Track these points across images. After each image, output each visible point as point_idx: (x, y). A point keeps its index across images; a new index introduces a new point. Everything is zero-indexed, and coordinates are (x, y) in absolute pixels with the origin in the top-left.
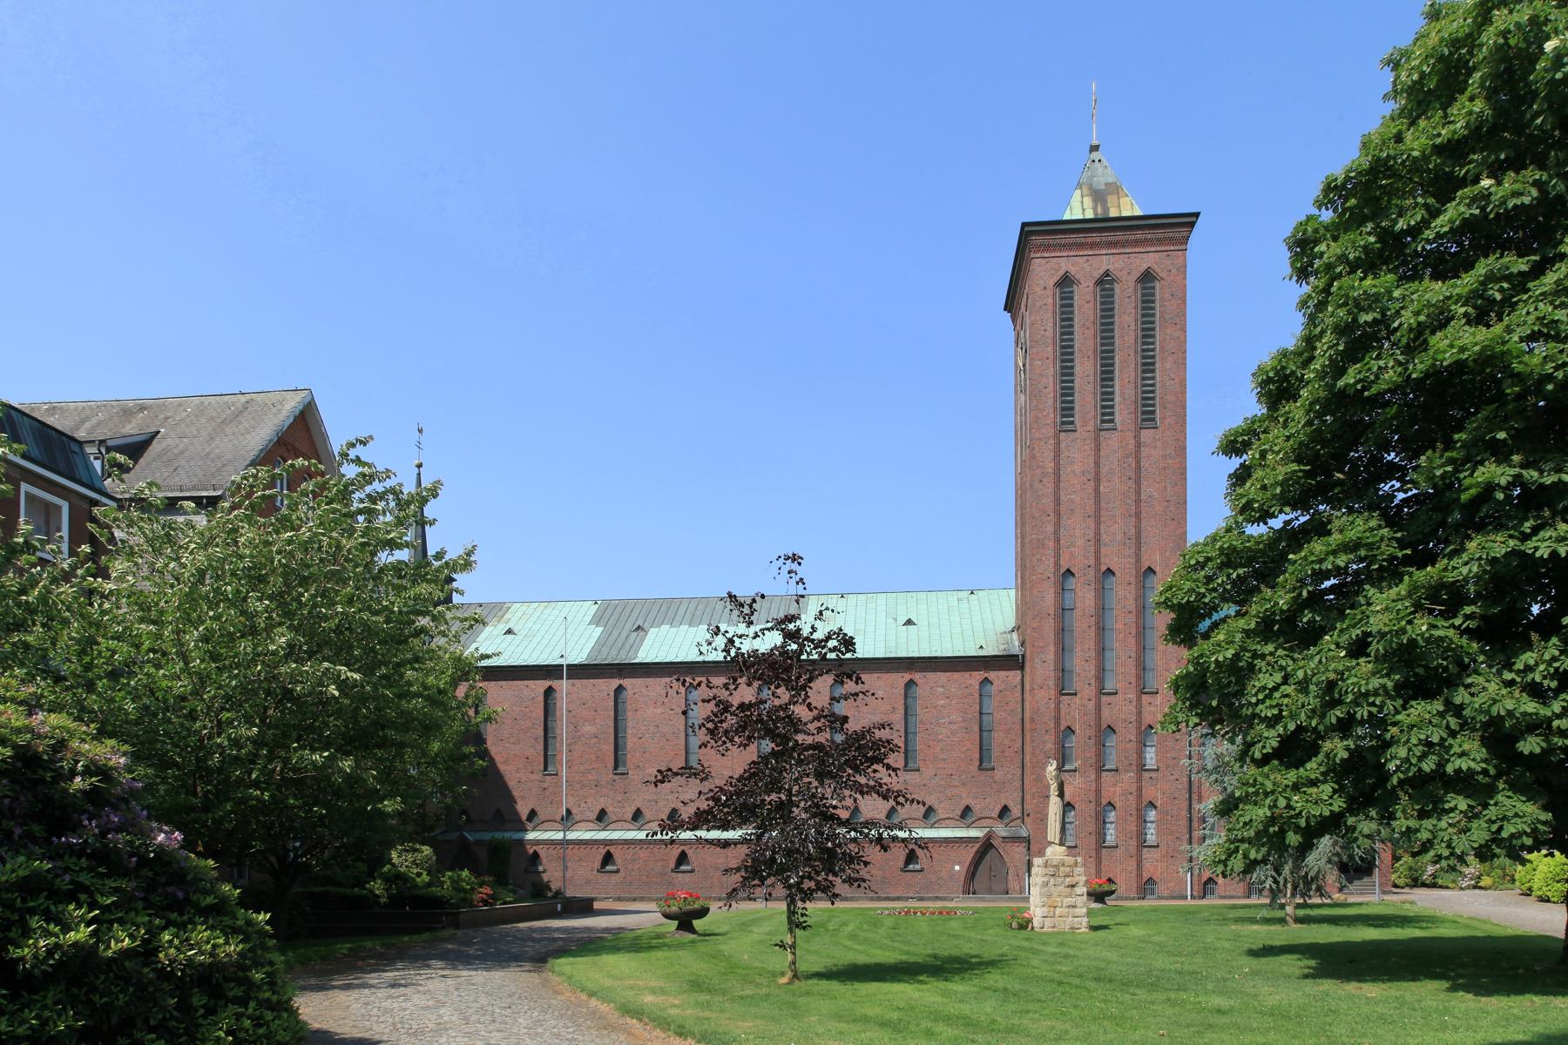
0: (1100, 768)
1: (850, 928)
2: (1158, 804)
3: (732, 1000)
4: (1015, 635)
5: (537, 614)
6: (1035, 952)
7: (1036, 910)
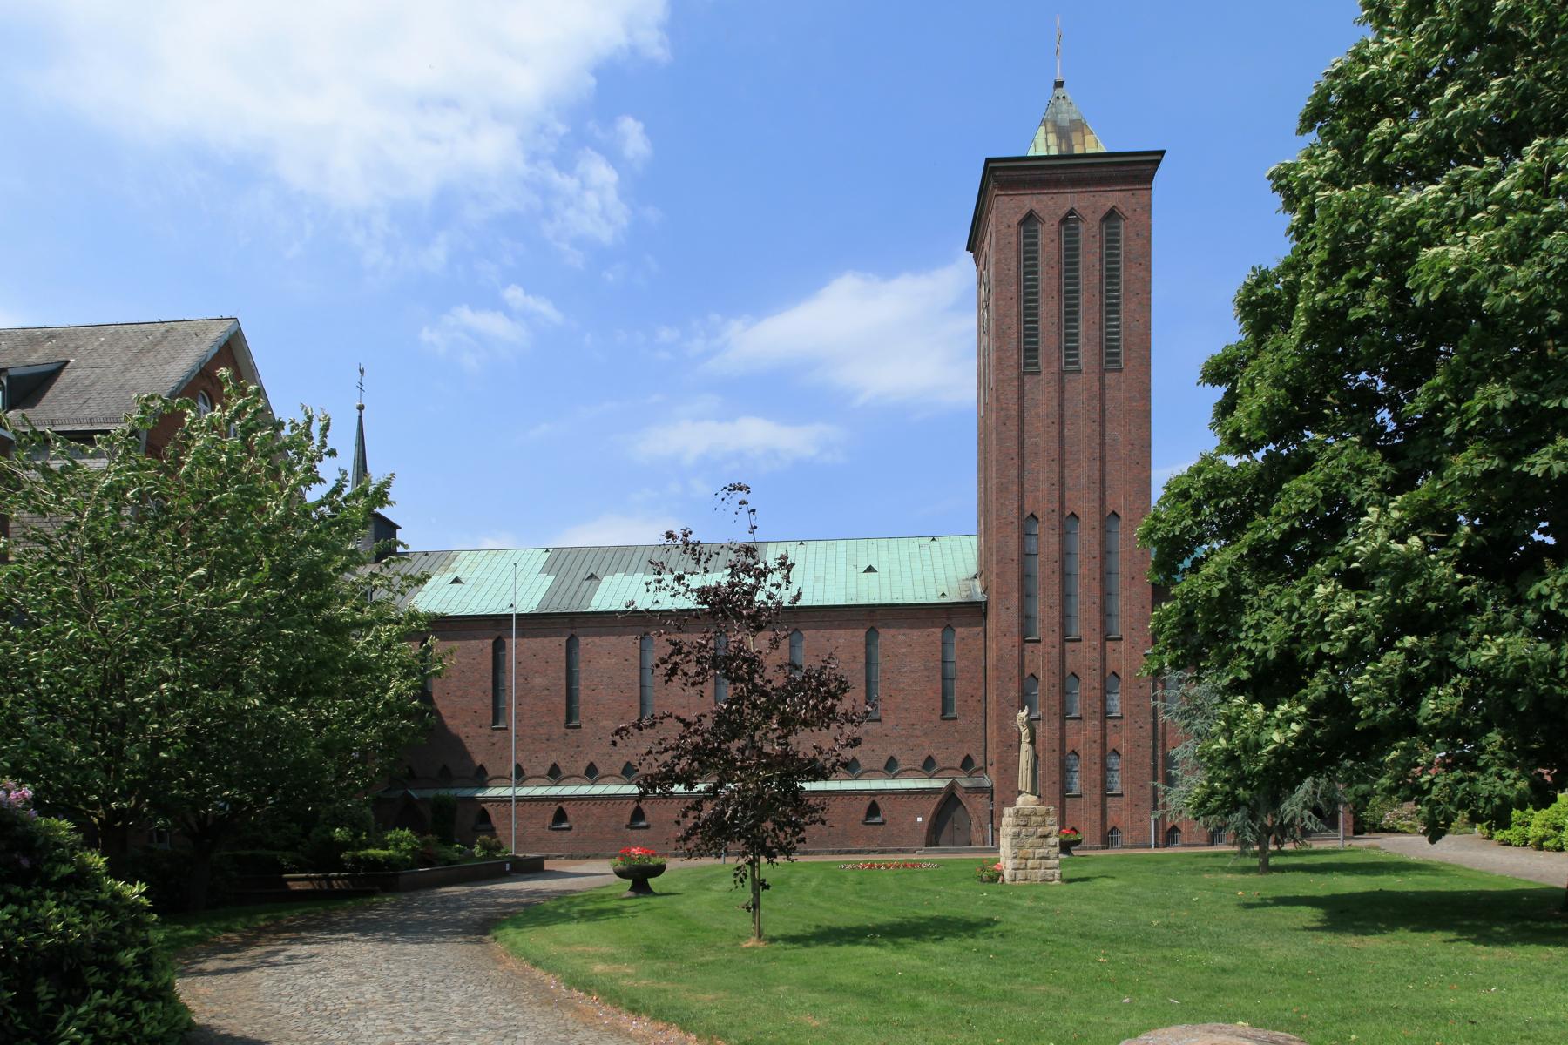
0: (1064, 716)
1: (814, 883)
2: (1122, 752)
3: (692, 968)
4: (977, 582)
5: (485, 562)
6: (1011, 907)
7: (1006, 861)
